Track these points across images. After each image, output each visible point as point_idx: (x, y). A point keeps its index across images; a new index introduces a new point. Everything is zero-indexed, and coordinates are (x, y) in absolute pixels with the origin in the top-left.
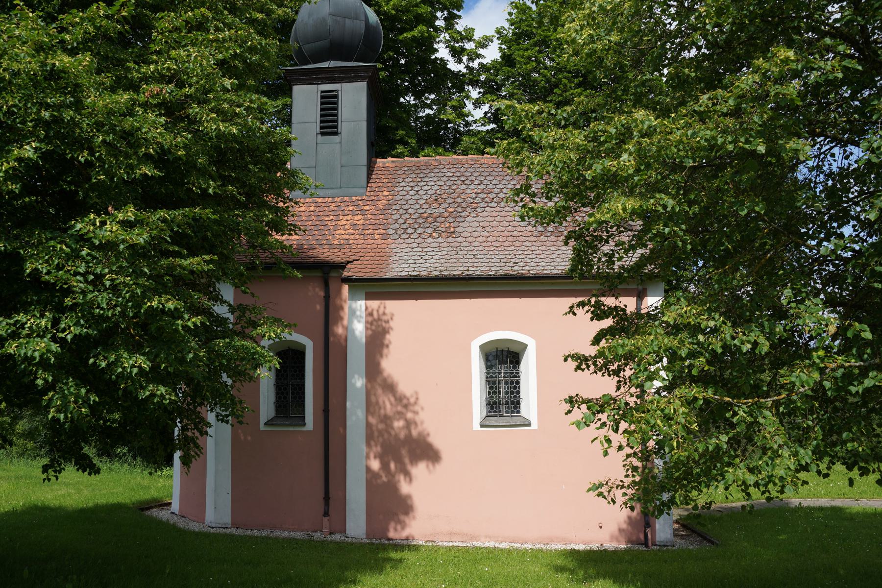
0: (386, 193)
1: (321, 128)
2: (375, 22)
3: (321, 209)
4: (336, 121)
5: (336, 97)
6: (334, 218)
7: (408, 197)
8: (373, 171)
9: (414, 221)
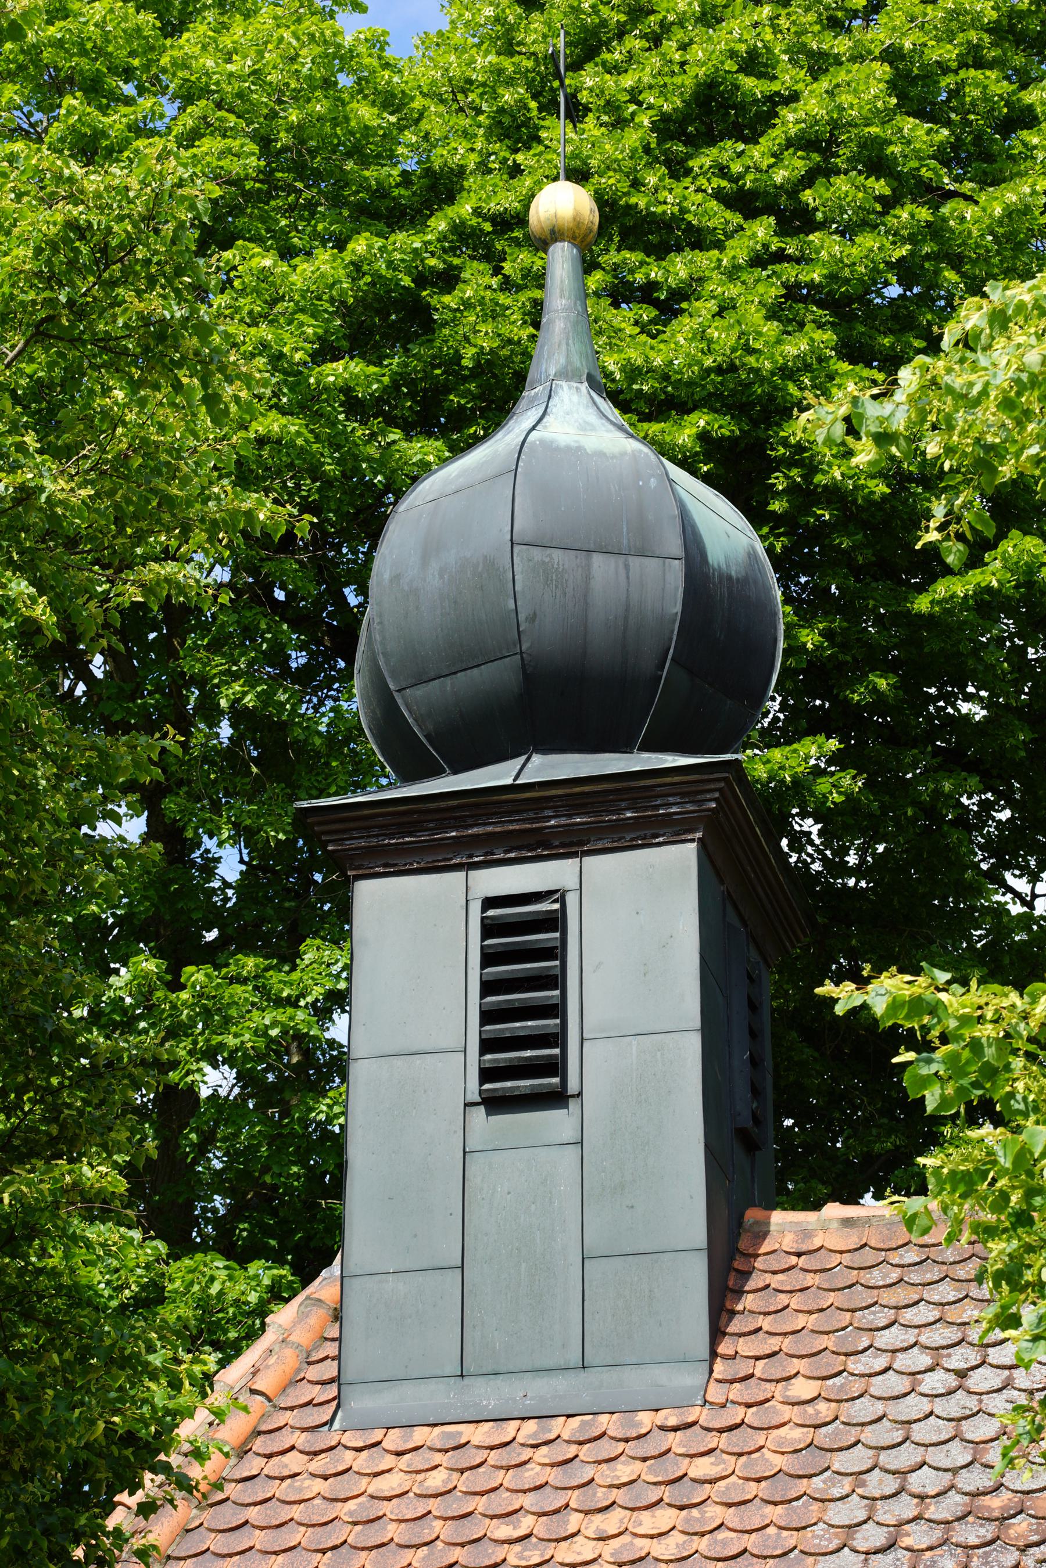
0: (803, 1389)
1: (487, 1075)
2: (741, 554)
3: (482, 1479)
4: (558, 1039)
5: (555, 922)
6: (542, 1527)
7: (915, 1407)
8: (746, 1275)
9: (938, 1534)
